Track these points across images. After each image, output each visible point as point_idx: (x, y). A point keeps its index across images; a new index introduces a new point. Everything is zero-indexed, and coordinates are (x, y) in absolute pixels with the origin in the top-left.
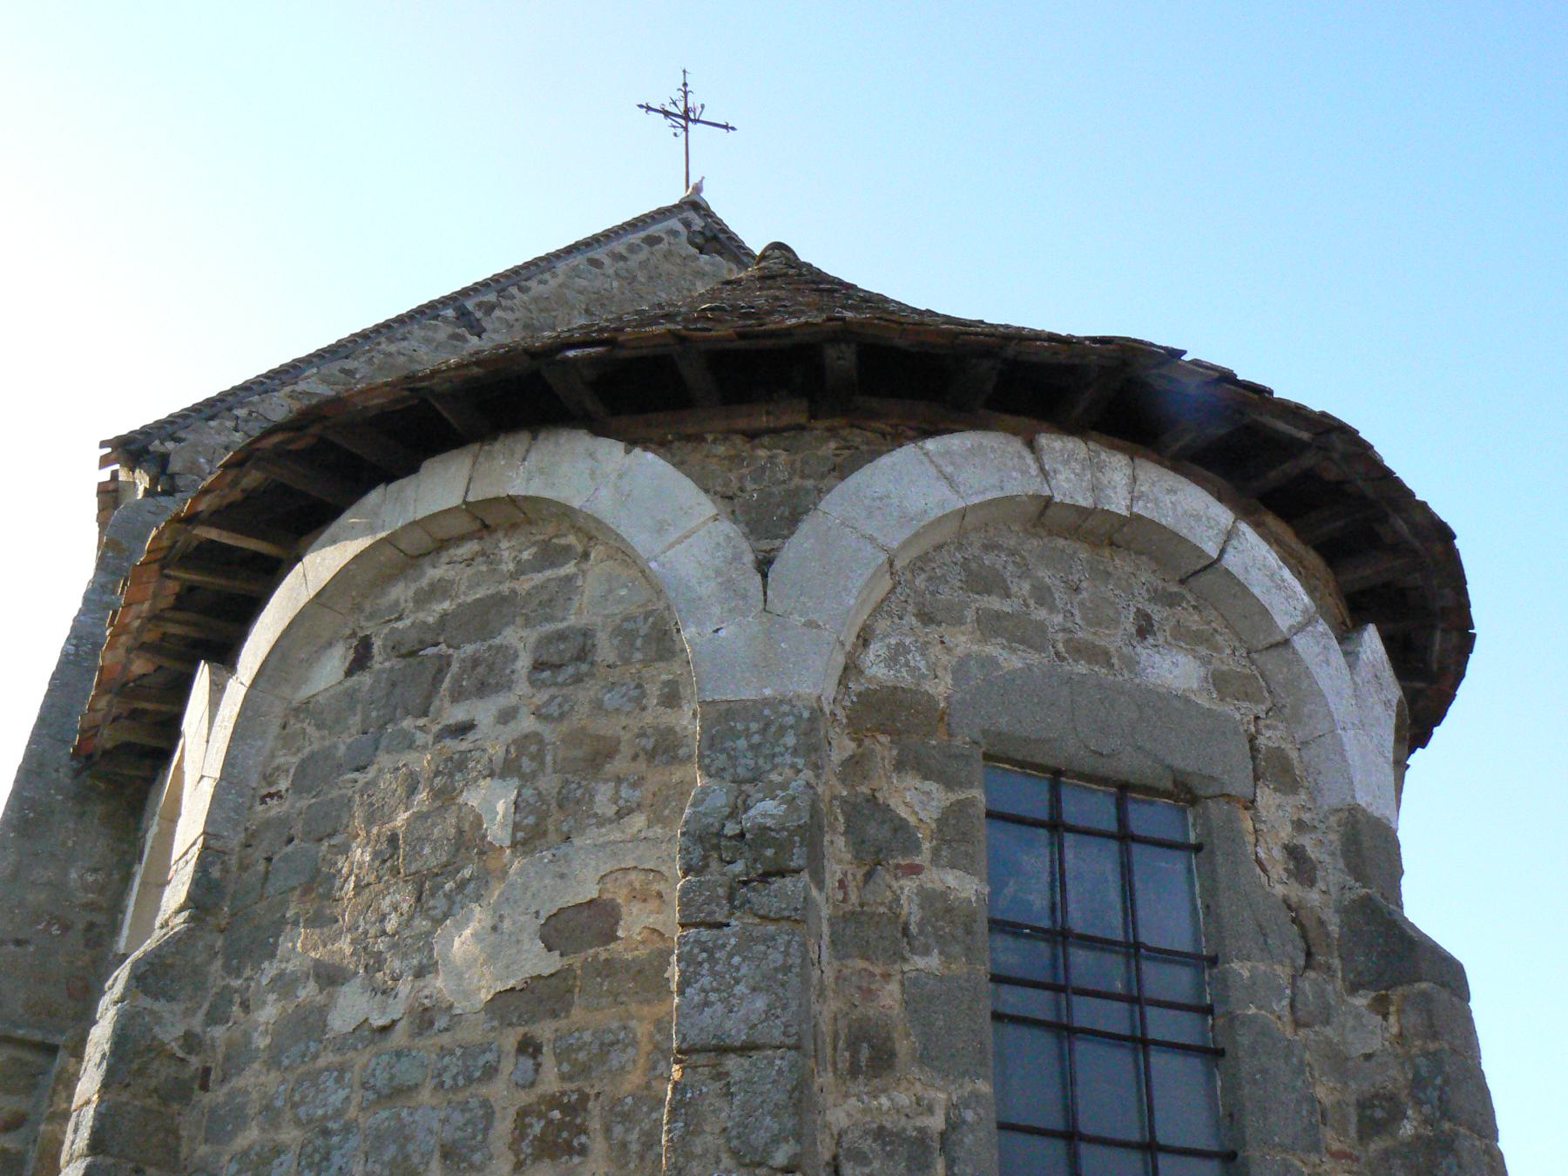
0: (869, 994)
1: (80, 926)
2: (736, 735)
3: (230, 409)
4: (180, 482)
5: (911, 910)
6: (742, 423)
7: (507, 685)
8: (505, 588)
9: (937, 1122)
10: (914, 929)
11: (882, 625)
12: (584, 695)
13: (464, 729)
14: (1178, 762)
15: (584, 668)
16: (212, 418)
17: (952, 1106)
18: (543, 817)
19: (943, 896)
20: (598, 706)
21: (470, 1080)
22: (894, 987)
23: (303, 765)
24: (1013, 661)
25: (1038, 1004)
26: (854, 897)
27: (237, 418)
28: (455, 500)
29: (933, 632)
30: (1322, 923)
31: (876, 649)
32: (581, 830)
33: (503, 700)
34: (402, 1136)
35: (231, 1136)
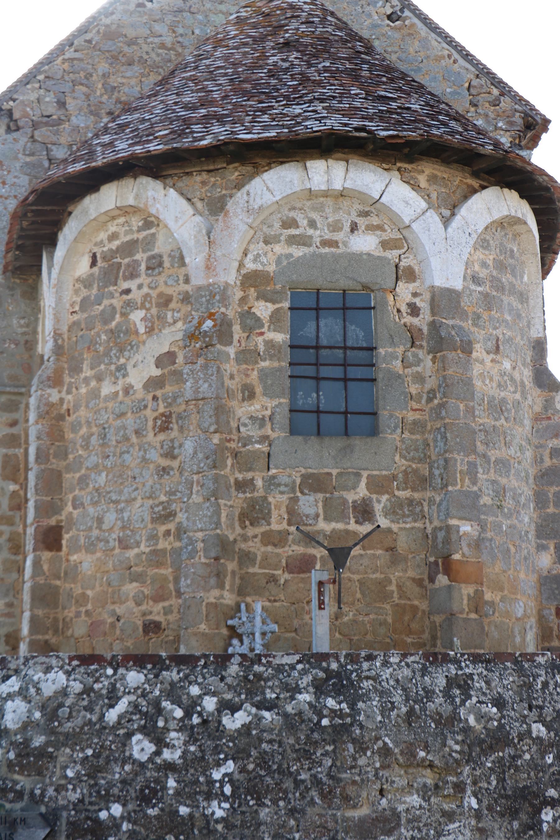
0: (247, 375)
1: (22, 342)
2: (202, 296)
3: (35, 77)
4: (20, 123)
5: (261, 348)
6: (206, 168)
7: (137, 276)
8: (135, 236)
9: (268, 413)
10: (261, 353)
11: (252, 247)
12: (161, 279)
13: (128, 291)
14: (364, 280)
15: (161, 269)
16: (28, 83)
17: (272, 408)
18: (153, 323)
19: (272, 341)
20: (166, 283)
21: (141, 410)
22: (255, 372)
23: (81, 301)
24: (298, 252)
25: (310, 371)
26: (243, 344)
27: (40, 81)
28: (113, 206)
29: (269, 247)
30: (420, 330)
31: (250, 256)
32: (164, 327)
33: (138, 281)
34: (124, 428)
35: (79, 430)
